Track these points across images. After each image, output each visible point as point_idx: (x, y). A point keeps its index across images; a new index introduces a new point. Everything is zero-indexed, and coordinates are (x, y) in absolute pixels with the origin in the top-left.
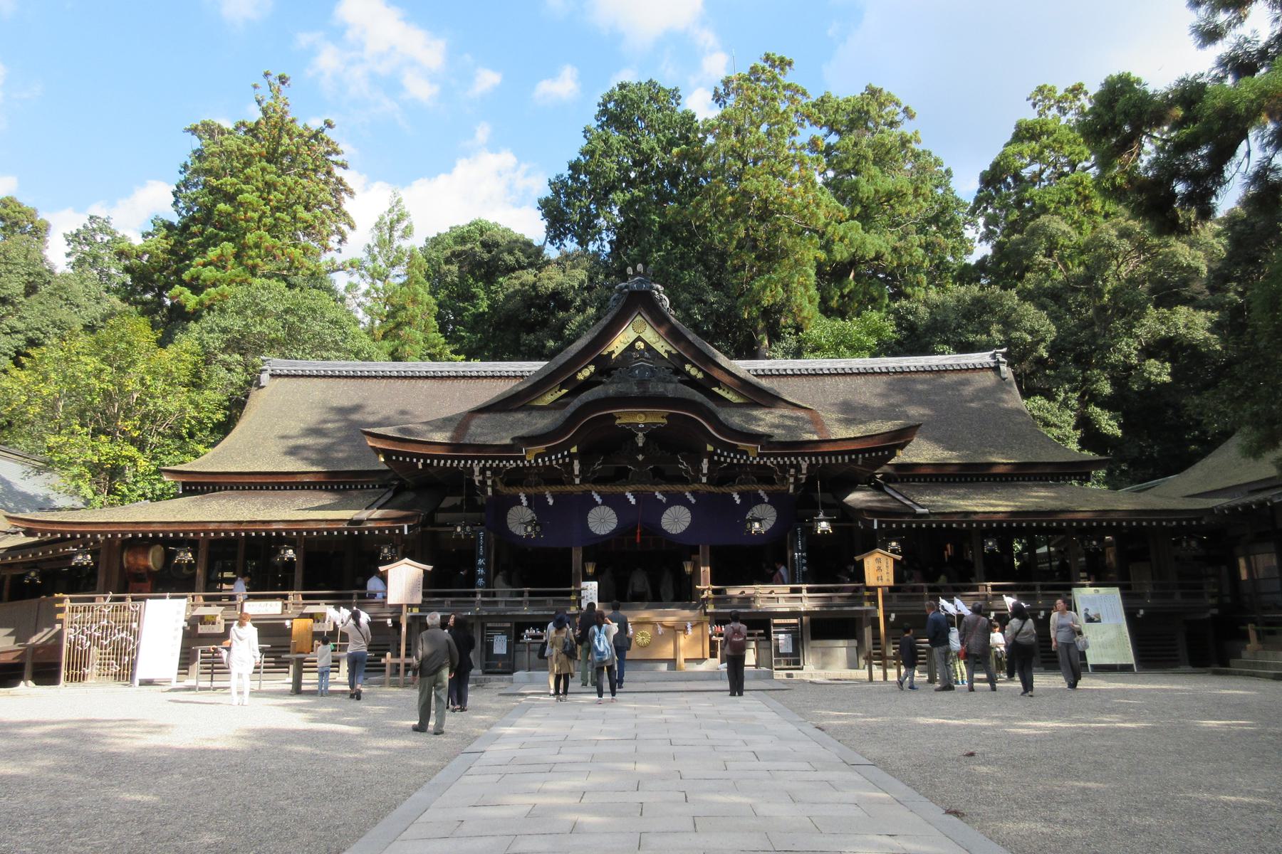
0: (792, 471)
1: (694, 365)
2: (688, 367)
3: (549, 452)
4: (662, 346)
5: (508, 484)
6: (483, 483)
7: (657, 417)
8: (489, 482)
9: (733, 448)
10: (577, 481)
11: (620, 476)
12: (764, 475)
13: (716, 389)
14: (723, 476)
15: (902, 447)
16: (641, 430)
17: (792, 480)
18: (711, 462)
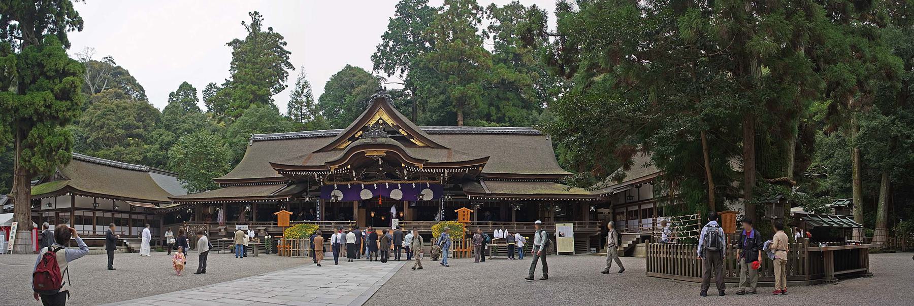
3: (340, 167)
4: (390, 122)
5: (330, 180)
7: (382, 153)
9: (413, 165)
11: (373, 178)
12: (432, 177)
14: (415, 177)
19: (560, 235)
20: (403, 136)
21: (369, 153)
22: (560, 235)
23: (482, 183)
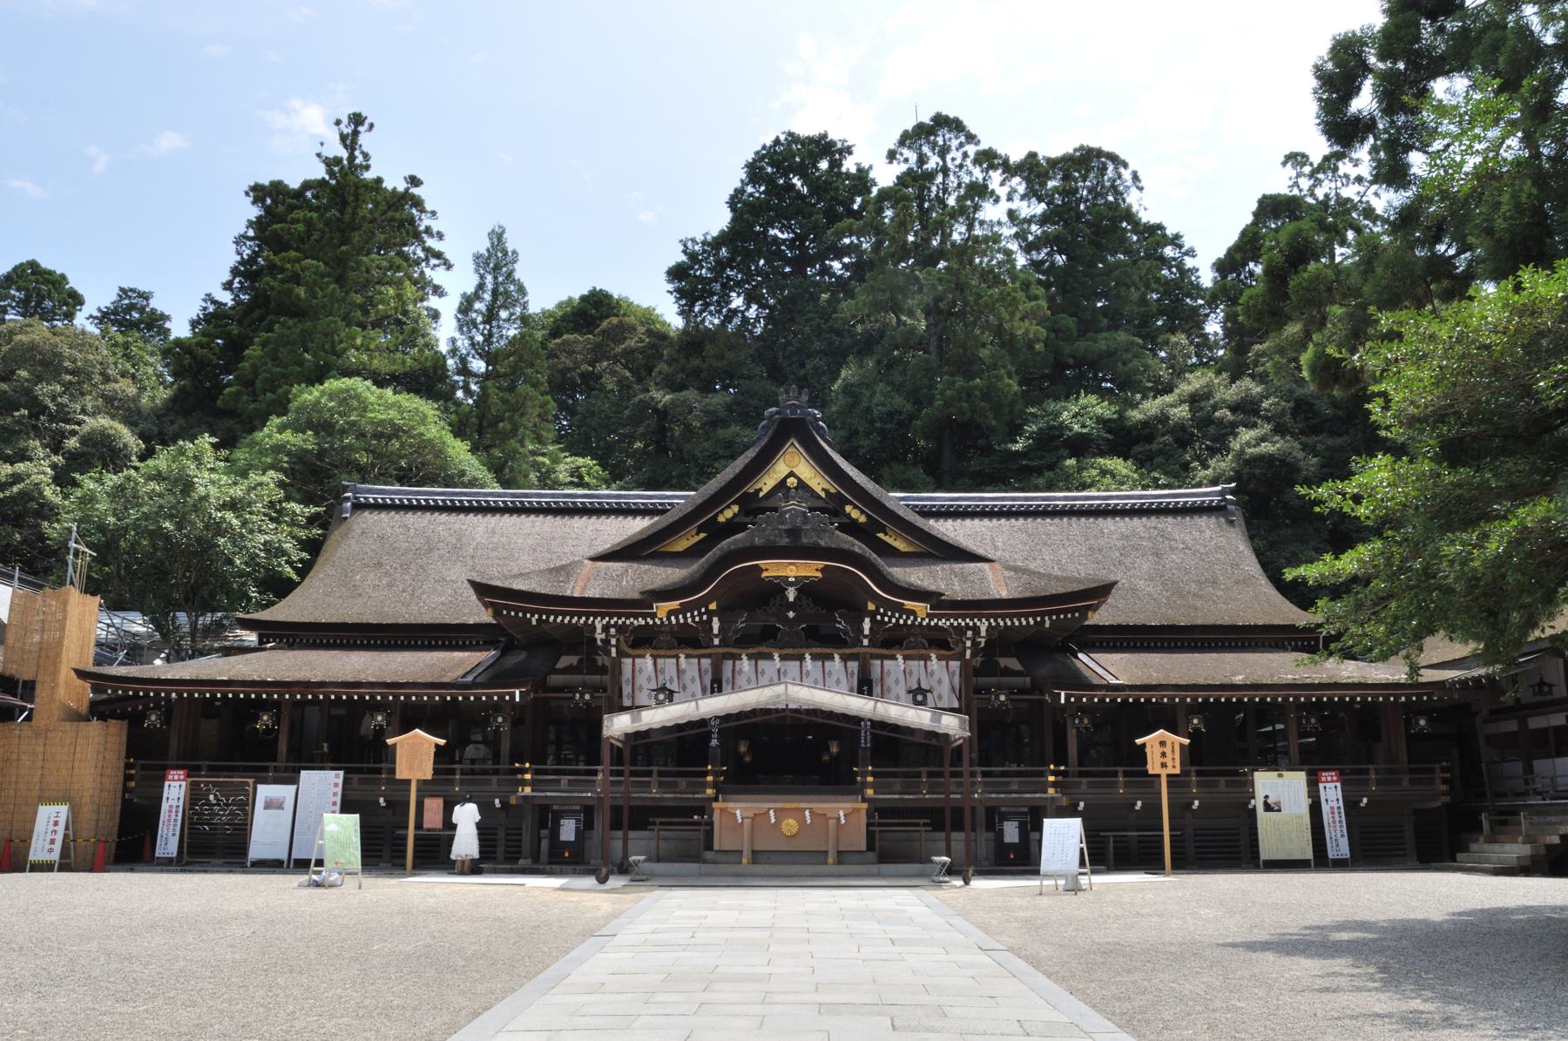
0: (970, 633)
1: (856, 507)
2: (848, 508)
3: (684, 609)
4: (818, 483)
6: (606, 642)
7: (810, 569)
8: (613, 641)
9: (900, 608)
10: (866, 642)
13: (881, 535)
15: (1095, 608)
16: (792, 584)
17: (969, 644)
18: (873, 621)
19: (1268, 807)
20: (855, 522)
21: (774, 568)
22: (1268, 807)
23: (1080, 655)
